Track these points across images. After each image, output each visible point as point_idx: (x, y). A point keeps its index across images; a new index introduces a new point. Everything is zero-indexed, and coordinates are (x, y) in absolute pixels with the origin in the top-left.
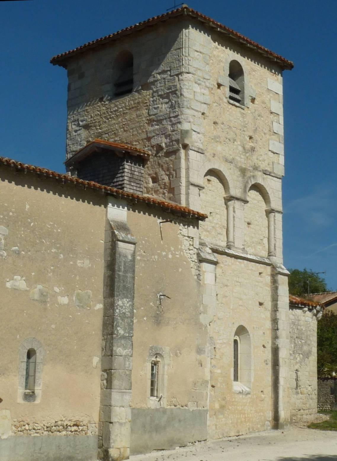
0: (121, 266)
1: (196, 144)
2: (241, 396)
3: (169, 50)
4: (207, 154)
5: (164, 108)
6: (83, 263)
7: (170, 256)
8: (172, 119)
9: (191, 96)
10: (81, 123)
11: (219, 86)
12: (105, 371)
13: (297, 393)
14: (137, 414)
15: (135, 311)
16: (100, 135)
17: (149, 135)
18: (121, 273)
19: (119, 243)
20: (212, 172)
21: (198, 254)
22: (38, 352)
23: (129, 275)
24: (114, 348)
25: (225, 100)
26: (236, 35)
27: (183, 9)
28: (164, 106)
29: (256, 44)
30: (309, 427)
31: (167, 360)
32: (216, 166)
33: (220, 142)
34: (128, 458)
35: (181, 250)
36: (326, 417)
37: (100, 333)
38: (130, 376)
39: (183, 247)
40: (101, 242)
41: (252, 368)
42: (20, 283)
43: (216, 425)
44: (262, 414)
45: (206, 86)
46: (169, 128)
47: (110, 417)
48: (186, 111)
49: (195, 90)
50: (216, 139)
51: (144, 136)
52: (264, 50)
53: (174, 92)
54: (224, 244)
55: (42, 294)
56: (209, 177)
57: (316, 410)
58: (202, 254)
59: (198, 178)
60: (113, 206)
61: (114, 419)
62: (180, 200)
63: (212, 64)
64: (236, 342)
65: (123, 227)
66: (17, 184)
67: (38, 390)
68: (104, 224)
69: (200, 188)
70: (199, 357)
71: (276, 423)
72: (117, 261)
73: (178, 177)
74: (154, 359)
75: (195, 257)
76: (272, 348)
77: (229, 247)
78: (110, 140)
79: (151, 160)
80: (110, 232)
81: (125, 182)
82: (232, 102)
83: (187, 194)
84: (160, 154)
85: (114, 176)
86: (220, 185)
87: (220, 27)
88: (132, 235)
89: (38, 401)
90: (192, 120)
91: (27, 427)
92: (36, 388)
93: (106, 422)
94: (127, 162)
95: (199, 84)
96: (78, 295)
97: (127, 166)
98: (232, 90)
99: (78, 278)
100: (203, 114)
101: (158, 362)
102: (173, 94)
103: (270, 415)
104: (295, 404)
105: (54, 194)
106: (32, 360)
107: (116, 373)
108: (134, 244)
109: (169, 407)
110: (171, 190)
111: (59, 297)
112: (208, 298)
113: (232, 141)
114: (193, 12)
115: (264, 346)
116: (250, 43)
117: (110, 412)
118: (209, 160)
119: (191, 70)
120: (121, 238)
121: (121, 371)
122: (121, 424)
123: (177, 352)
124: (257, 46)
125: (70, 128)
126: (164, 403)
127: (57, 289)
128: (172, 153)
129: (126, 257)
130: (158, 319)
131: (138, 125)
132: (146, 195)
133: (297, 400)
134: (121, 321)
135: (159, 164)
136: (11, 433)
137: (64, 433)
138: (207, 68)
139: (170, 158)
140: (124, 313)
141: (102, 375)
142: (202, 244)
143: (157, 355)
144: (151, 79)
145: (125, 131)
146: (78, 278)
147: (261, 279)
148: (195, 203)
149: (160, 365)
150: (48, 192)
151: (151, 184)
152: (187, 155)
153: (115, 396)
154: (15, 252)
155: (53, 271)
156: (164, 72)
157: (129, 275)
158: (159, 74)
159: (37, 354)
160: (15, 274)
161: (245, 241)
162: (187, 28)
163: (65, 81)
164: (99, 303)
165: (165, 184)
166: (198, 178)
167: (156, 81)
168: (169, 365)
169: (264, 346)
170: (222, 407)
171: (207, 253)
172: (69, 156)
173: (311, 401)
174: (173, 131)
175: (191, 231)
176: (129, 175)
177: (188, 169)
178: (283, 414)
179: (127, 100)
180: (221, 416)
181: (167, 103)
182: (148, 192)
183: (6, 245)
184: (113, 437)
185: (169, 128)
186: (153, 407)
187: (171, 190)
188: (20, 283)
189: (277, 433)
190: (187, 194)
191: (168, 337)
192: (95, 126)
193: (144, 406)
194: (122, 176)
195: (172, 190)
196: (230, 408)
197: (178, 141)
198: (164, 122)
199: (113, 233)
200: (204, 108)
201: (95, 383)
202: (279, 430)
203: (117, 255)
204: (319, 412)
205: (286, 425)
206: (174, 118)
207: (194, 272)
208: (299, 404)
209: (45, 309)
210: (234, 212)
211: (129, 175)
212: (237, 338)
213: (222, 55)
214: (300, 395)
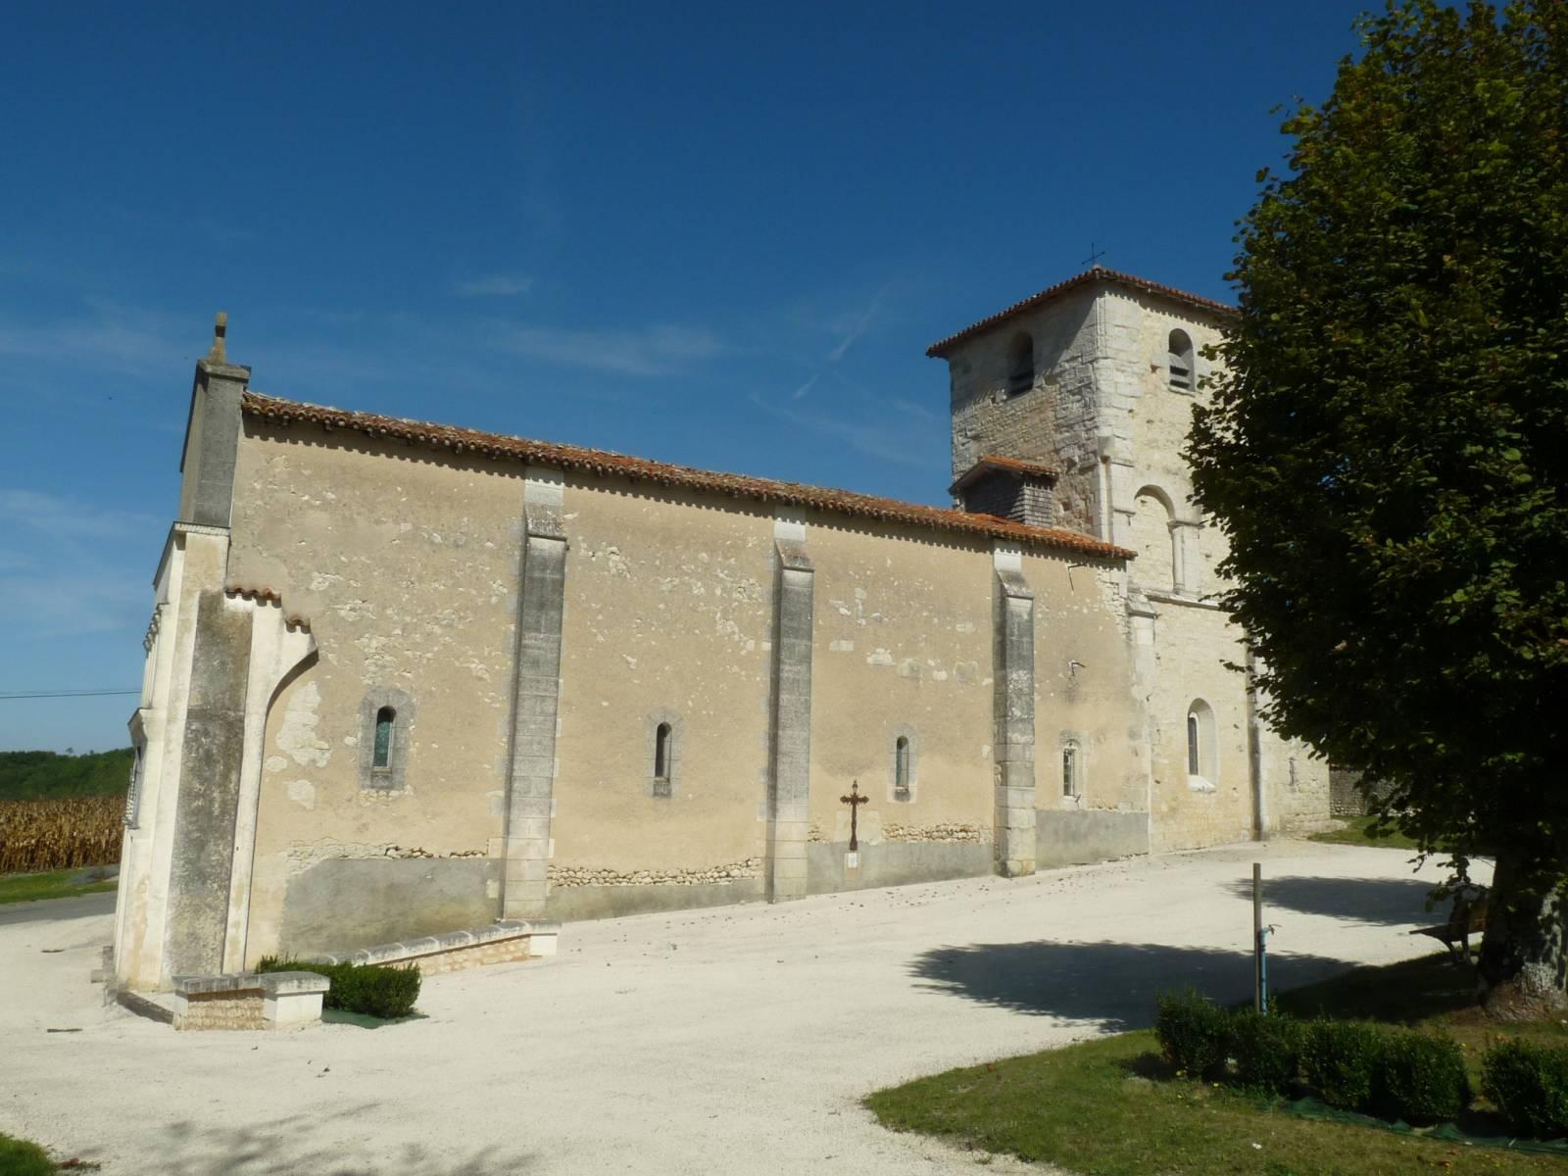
0: (1014, 631)
1: (1120, 455)
2: (1201, 795)
3: (1078, 327)
4: (1139, 467)
5: (1075, 407)
6: (964, 628)
7: (1085, 611)
8: (1087, 423)
9: (1112, 390)
10: (969, 433)
11: (1154, 368)
12: (998, 763)
13: (1293, 791)
14: (1044, 819)
15: (1037, 685)
16: (994, 448)
17: (1058, 446)
18: (1014, 638)
19: (1010, 599)
20: (1147, 491)
21: (1127, 606)
22: (910, 740)
23: (1025, 639)
24: (1009, 734)
25: (1165, 388)
26: (1177, 294)
27: (1094, 271)
28: (1076, 405)
29: (1208, 301)
30: (1310, 838)
31: (1085, 748)
32: (1153, 482)
33: (1158, 448)
34: (1033, 873)
35: (1102, 601)
36: (1342, 825)
37: (990, 715)
38: (1031, 769)
39: (1104, 598)
40: (988, 599)
41: (1218, 756)
42: (884, 656)
43: (1164, 834)
44: (1235, 819)
45: (1134, 373)
46: (1084, 435)
47: (1007, 822)
48: (1105, 411)
49: (1116, 380)
50: (1152, 444)
51: (1051, 447)
52: (1222, 308)
53: (1088, 386)
54: (1170, 587)
55: (912, 669)
56: (1143, 497)
57: (1328, 815)
58: (1132, 605)
59: (1125, 499)
60: (1002, 551)
61: (1012, 824)
62: (1101, 532)
63: (1143, 339)
64: (1191, 721)
65: (1016, 578)
66: (874, 535)
67: (913, 787)
68: (991, 571)
69: (1129, 514)
70: (1132, 743)
71: (1258, 832)
72: (1009, 623)
73: (1098, 502)
74: (1067, 747)
75: (1122, 610)
76: (1249, 729)
77: (1176, 592)
78: (1007, 457)
79: (1061, 480)
80: (998, 586)
81: (1026, 512)
82: (1174, 388)
83: (1111, 524)
84: (1072, 472)
85: (1011, 505)
86: (1160, 507)
87: (1151, 286)
88: (1028, 587)
89: (913, 800)
90: (1113, 422)
91: (901, 832)
92: (910, 785)
93: (1003, 828)
94: (1028, 485)
95: (1123, 371)
96: (959, 668)
97: (1028, 491)
98: (1174, 370)
99: (958, 647)
100: (1131, 411)
101: (1073, 751)
102: (1086, 389)
103: (1248, 821)
104: (1290, 806)
105: (923, 542)
106: (904, 750)
107: (1014, 765)
108: (1031, 599)
109: (1091, 809)
110: (1089, 520)
111: (935, 673)
112: (1144, 664)
113: (1177, 443)
114: (1108, 273)
115: (1236, 726)
116: (1200, 302)
117: (1007, 815)
118: (1142, 475)
119: (1110, 353)
120: (1012, 593)
121: (1019, 763)
122: (1022, 830)
123: (1100, 736)
124: (1211, 304)
125: (955, 441)
126: (1084, 804)
127: (931, 663)
128: (1088, 469)
129: (1020, 616)
130: (1070, 695)
131: (1042, 432)
132: (1056, 528)
133: (1293, 801)
134: (1016, 700)
135: (1072, 485)
136: (881, 839)
137: (949, 840)
138: (1135, 347)
139: (1086, 476)
140: (1021, 690)
141: (996, 768)
142: (1134, 590)
143: (1071, 741)
144: (1057, 370)
145: (1025, 441)
146: (958, 647)
147: (1229, 633)
148: (1117, 534)
149: (1077, 755)
150: (915, 541)
151: (1062, 512)
152: (1108, 471)
153: (1013, 796)
154: (876, 619)
155: (926, 640)
156: (1074, 359)
157: (1025, 639)
158: (1067, 361)
159: (910, 744)
160: (876, 646)
161: (1202, 581)
162: (1102, 295)
163: (947, 378)
164: (988, 677)
165: (1080, 513)
166: (1125, 499)
167: (1064, 371)
168: (1088, 754)
169: (1236, 726)
170: (1173, 810)
171: (1141, 603)
172: (957, 478)
173: (1317, 802)
174: (1088, 439)
175: (1115, 574)
176: (1031, 503)
177: (1110, 490)
178: (1267, 820)
179: (1026, 400)
180: (1172, 822)
181: (1078, 401)
182: (1058, 524)
183: (864, 611)
184: (1011, 846)
185: (1084, 435)
186: (1068, 809)
187: (1089, 520)
188: (884, 656)
189: (1258, 846)
190: (1111, 524)
191: (1084, 719)
192: (987, 437)
193: (1055, 808)
194: (1022, 505)
195: (1090, 519)
196: (1185, 810)
197: (1094, 452)
198: (1076, 427)
199: (1002, 587)
200: (1131, 403)
201: (988, 777)
202: (1262, 843)
203: (1008, 615)
204: (1333, 817)
205: (1274, 835)
206: (1089, 422)
207: (1121, 629)
208: (1296, 805)
209: (917, 688)
210: (1183, 542)
211: (1031, 503)
212: (1193, 715)
213: (1158, 325)
214: (1298, 794)
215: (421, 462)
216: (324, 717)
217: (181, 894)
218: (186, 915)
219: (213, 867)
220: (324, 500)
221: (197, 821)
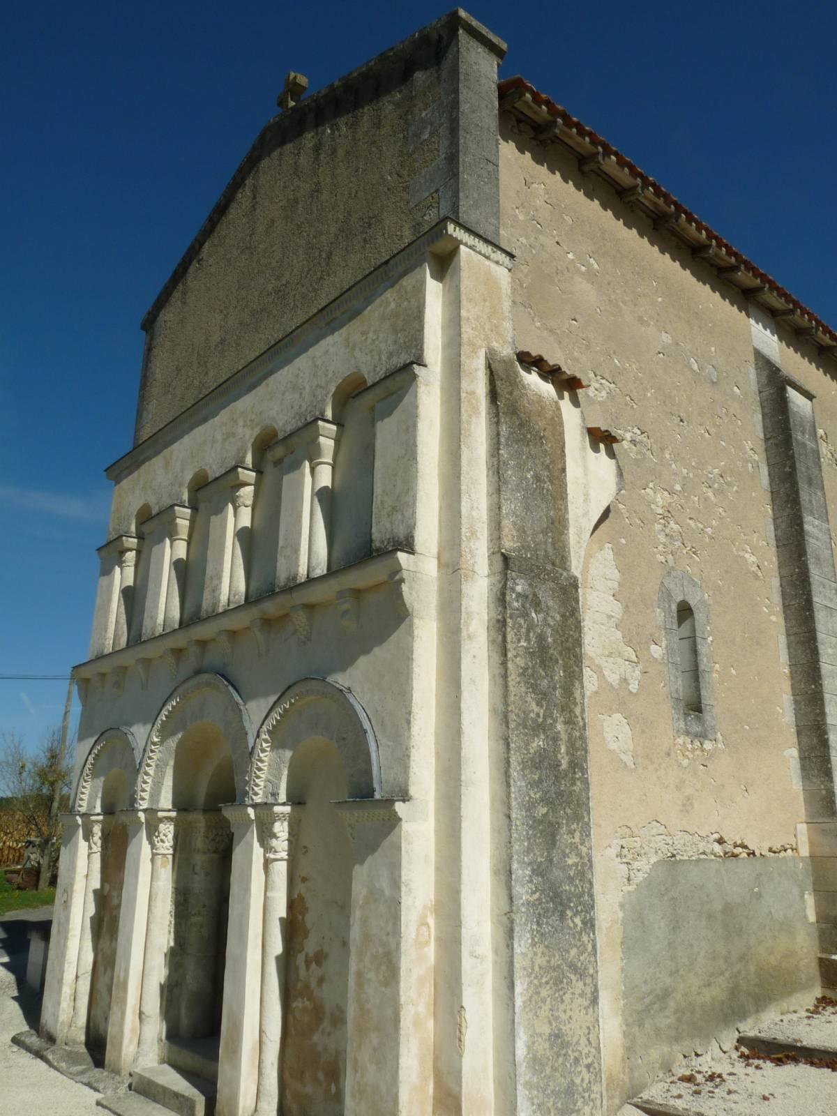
215: (667, 256)
216: (627, 606)
217: (534, 945)
218: (544, 992)
219: (571, 879)
220: (589, 266)
221: (540, 781)
